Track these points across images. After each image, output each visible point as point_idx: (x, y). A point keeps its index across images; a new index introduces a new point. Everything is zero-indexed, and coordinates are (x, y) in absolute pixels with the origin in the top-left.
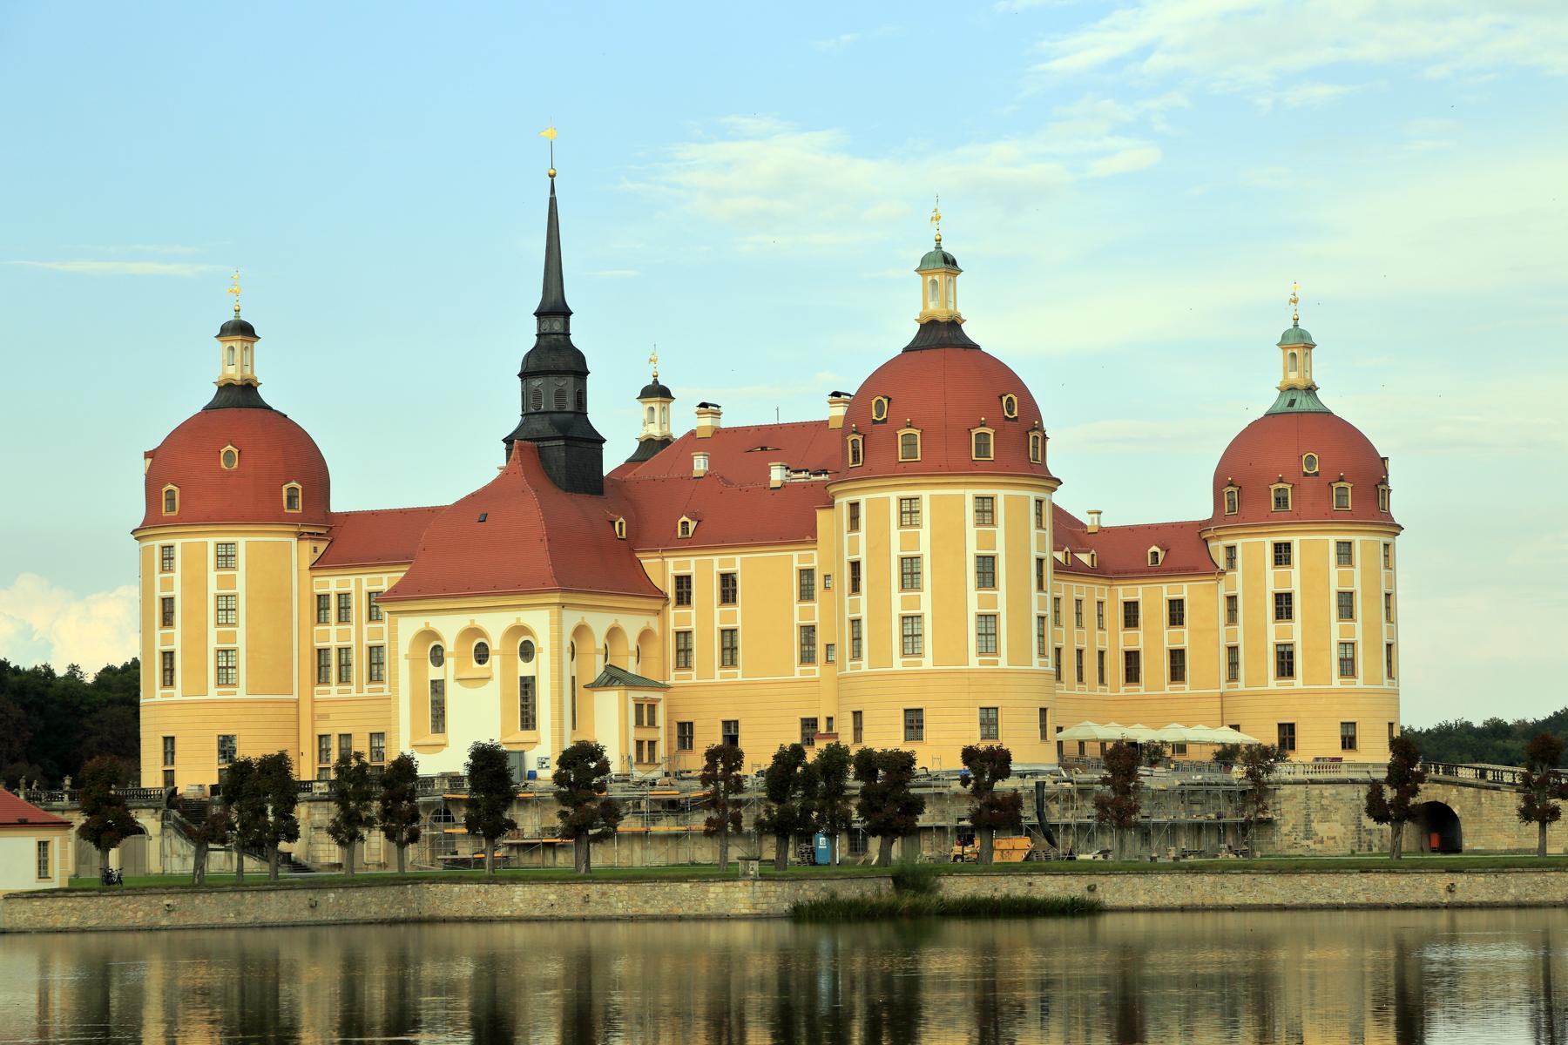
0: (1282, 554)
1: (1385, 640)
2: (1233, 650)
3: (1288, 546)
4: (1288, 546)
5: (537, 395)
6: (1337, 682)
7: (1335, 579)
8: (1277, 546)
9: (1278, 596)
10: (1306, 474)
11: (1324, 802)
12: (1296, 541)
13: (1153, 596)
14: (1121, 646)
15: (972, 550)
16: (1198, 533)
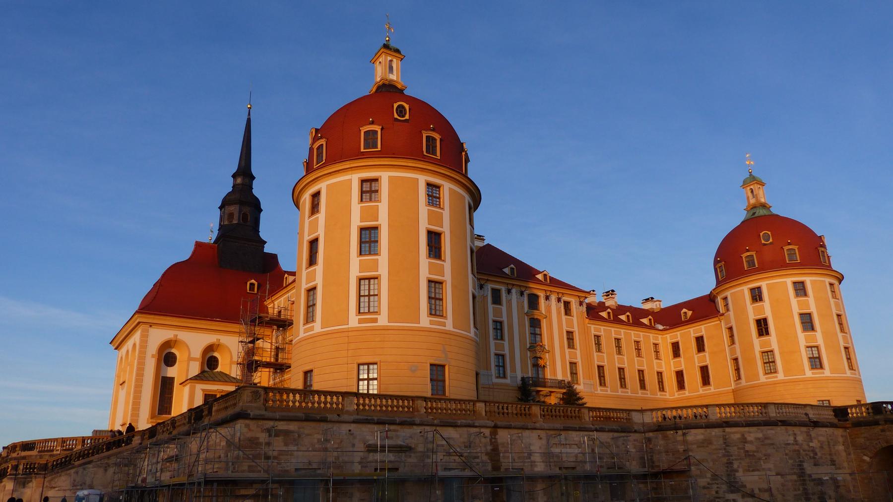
0: (757, 295)
1: (842, 344)
3: (759, 288)
4: (759, 288)
5: (231, 216)
6: (809, 373)
7: (795, 305)
8: (752, 290)
9: (758, 322)
10: (765, 245)
11: (748, 447)
12: (764, 285)
13: (686, 335)
14: (673, 369)
15: (356, 222)
16: (710, 299)
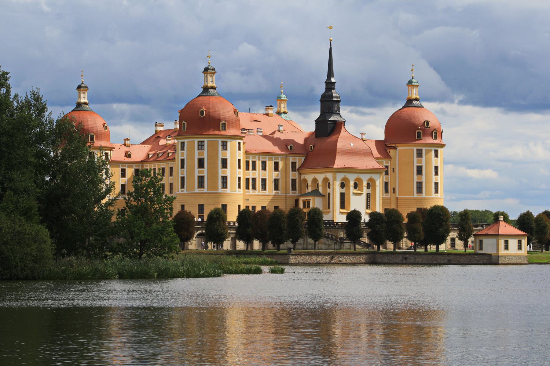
2: (183, 178)
3: (422, 150)
4: (422, 150)
